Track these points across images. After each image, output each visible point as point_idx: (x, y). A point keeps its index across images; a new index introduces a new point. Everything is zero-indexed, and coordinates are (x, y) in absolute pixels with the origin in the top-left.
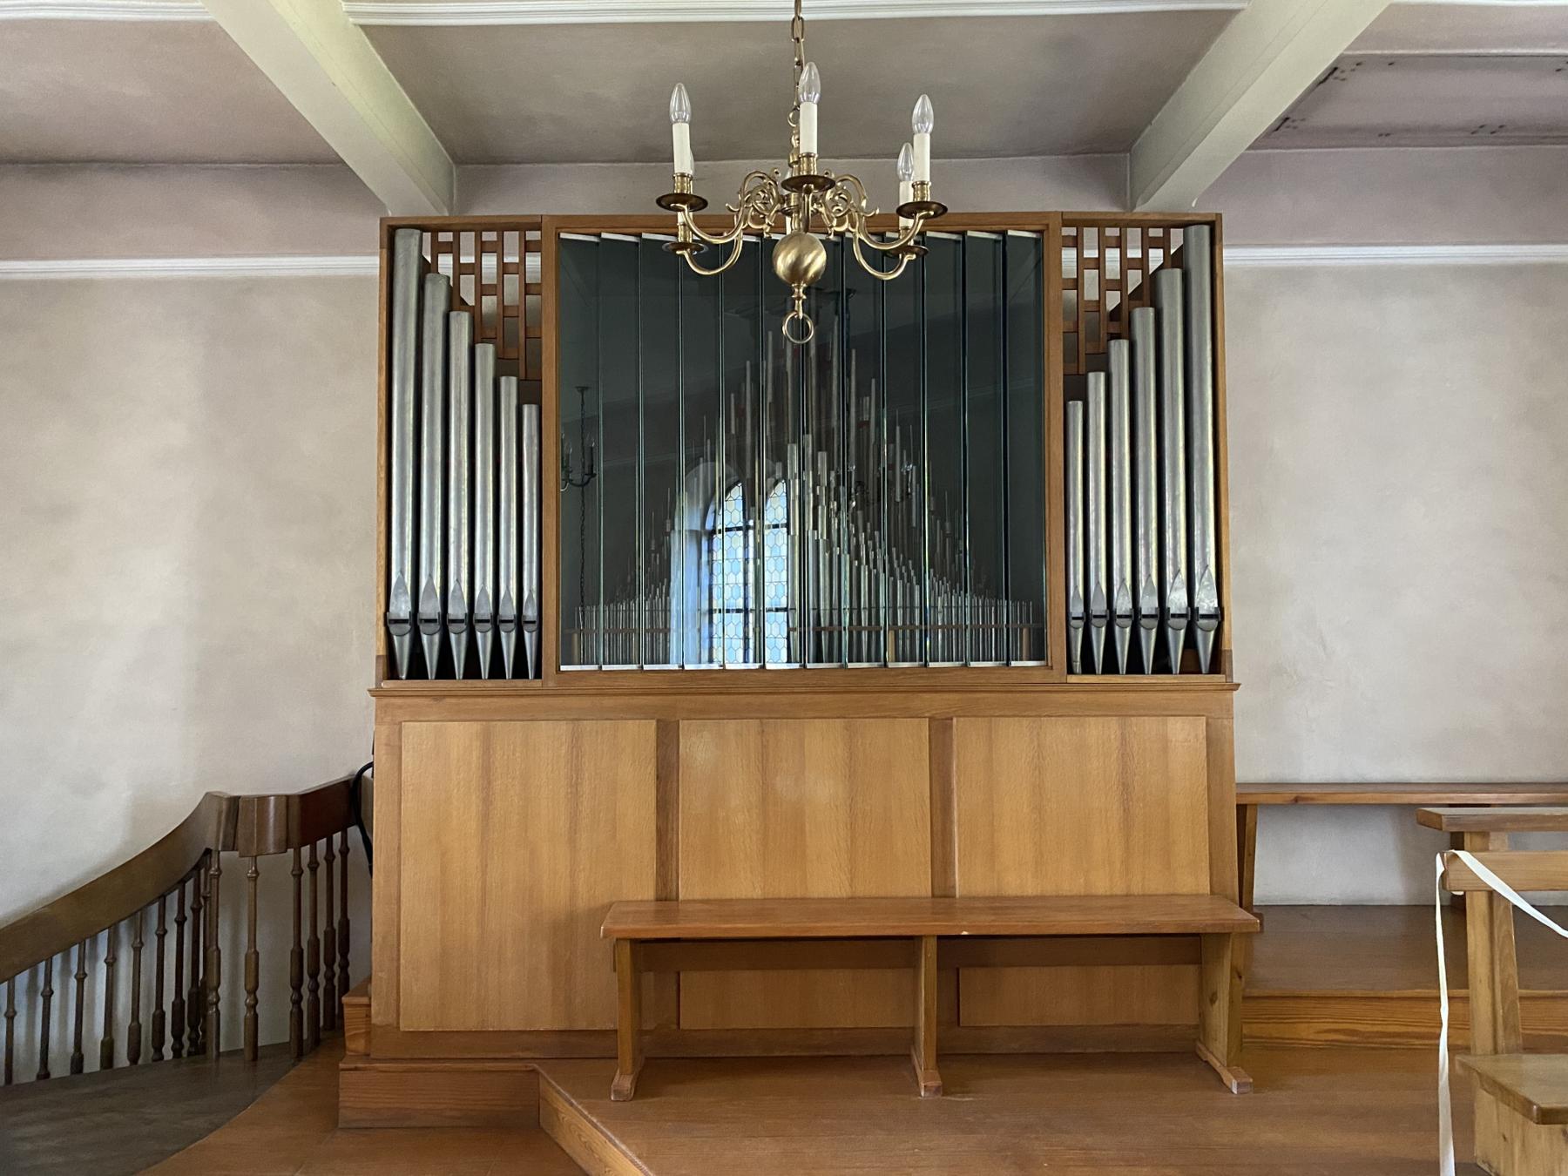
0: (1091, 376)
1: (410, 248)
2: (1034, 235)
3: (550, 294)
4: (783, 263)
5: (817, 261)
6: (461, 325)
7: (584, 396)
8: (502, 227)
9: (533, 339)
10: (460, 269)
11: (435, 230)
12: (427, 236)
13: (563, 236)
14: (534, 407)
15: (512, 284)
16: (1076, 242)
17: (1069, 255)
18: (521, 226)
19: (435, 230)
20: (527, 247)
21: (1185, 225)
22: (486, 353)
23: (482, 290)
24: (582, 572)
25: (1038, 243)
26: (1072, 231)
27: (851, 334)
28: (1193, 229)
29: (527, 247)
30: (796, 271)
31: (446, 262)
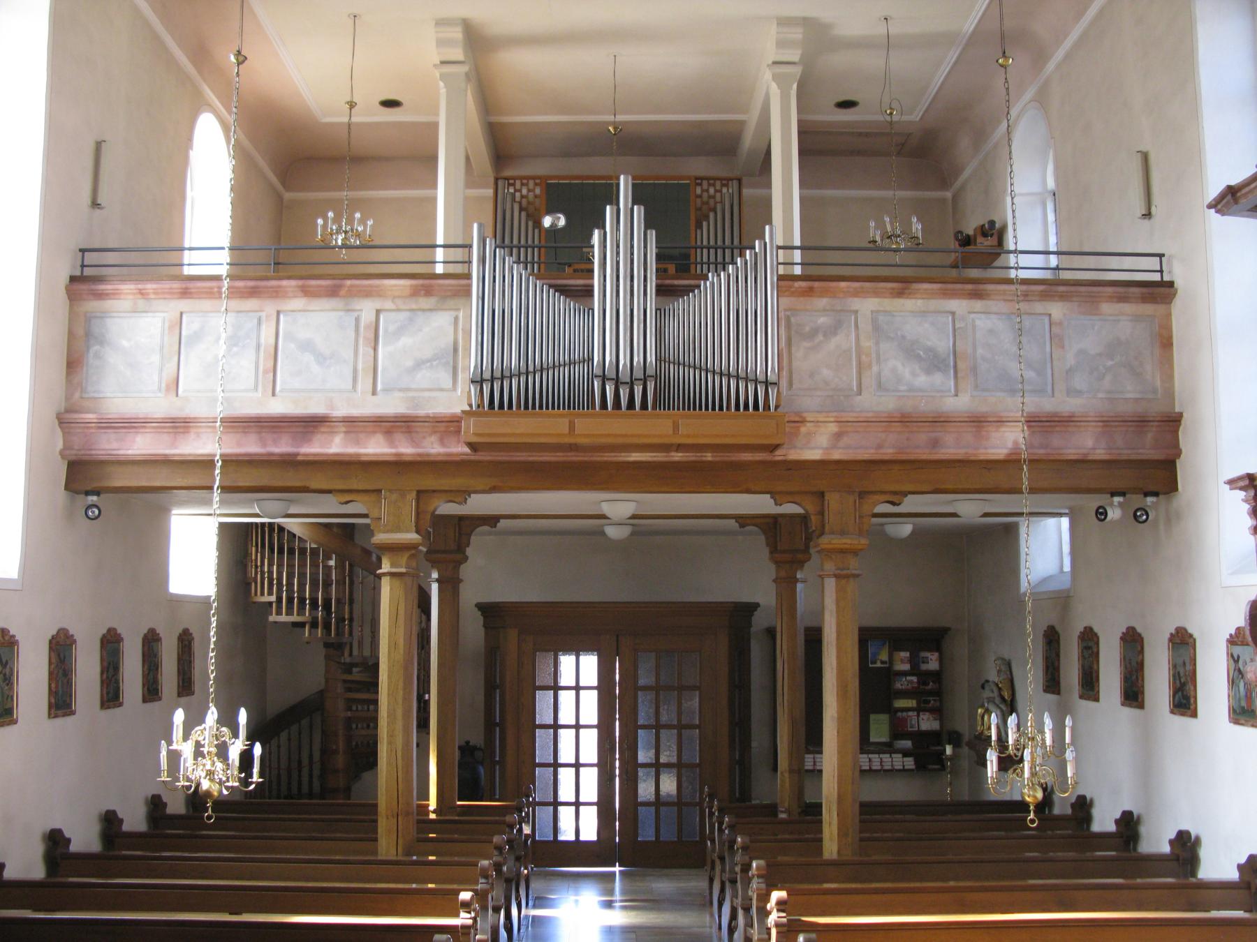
6: (516, 207)
22: (523, 214)
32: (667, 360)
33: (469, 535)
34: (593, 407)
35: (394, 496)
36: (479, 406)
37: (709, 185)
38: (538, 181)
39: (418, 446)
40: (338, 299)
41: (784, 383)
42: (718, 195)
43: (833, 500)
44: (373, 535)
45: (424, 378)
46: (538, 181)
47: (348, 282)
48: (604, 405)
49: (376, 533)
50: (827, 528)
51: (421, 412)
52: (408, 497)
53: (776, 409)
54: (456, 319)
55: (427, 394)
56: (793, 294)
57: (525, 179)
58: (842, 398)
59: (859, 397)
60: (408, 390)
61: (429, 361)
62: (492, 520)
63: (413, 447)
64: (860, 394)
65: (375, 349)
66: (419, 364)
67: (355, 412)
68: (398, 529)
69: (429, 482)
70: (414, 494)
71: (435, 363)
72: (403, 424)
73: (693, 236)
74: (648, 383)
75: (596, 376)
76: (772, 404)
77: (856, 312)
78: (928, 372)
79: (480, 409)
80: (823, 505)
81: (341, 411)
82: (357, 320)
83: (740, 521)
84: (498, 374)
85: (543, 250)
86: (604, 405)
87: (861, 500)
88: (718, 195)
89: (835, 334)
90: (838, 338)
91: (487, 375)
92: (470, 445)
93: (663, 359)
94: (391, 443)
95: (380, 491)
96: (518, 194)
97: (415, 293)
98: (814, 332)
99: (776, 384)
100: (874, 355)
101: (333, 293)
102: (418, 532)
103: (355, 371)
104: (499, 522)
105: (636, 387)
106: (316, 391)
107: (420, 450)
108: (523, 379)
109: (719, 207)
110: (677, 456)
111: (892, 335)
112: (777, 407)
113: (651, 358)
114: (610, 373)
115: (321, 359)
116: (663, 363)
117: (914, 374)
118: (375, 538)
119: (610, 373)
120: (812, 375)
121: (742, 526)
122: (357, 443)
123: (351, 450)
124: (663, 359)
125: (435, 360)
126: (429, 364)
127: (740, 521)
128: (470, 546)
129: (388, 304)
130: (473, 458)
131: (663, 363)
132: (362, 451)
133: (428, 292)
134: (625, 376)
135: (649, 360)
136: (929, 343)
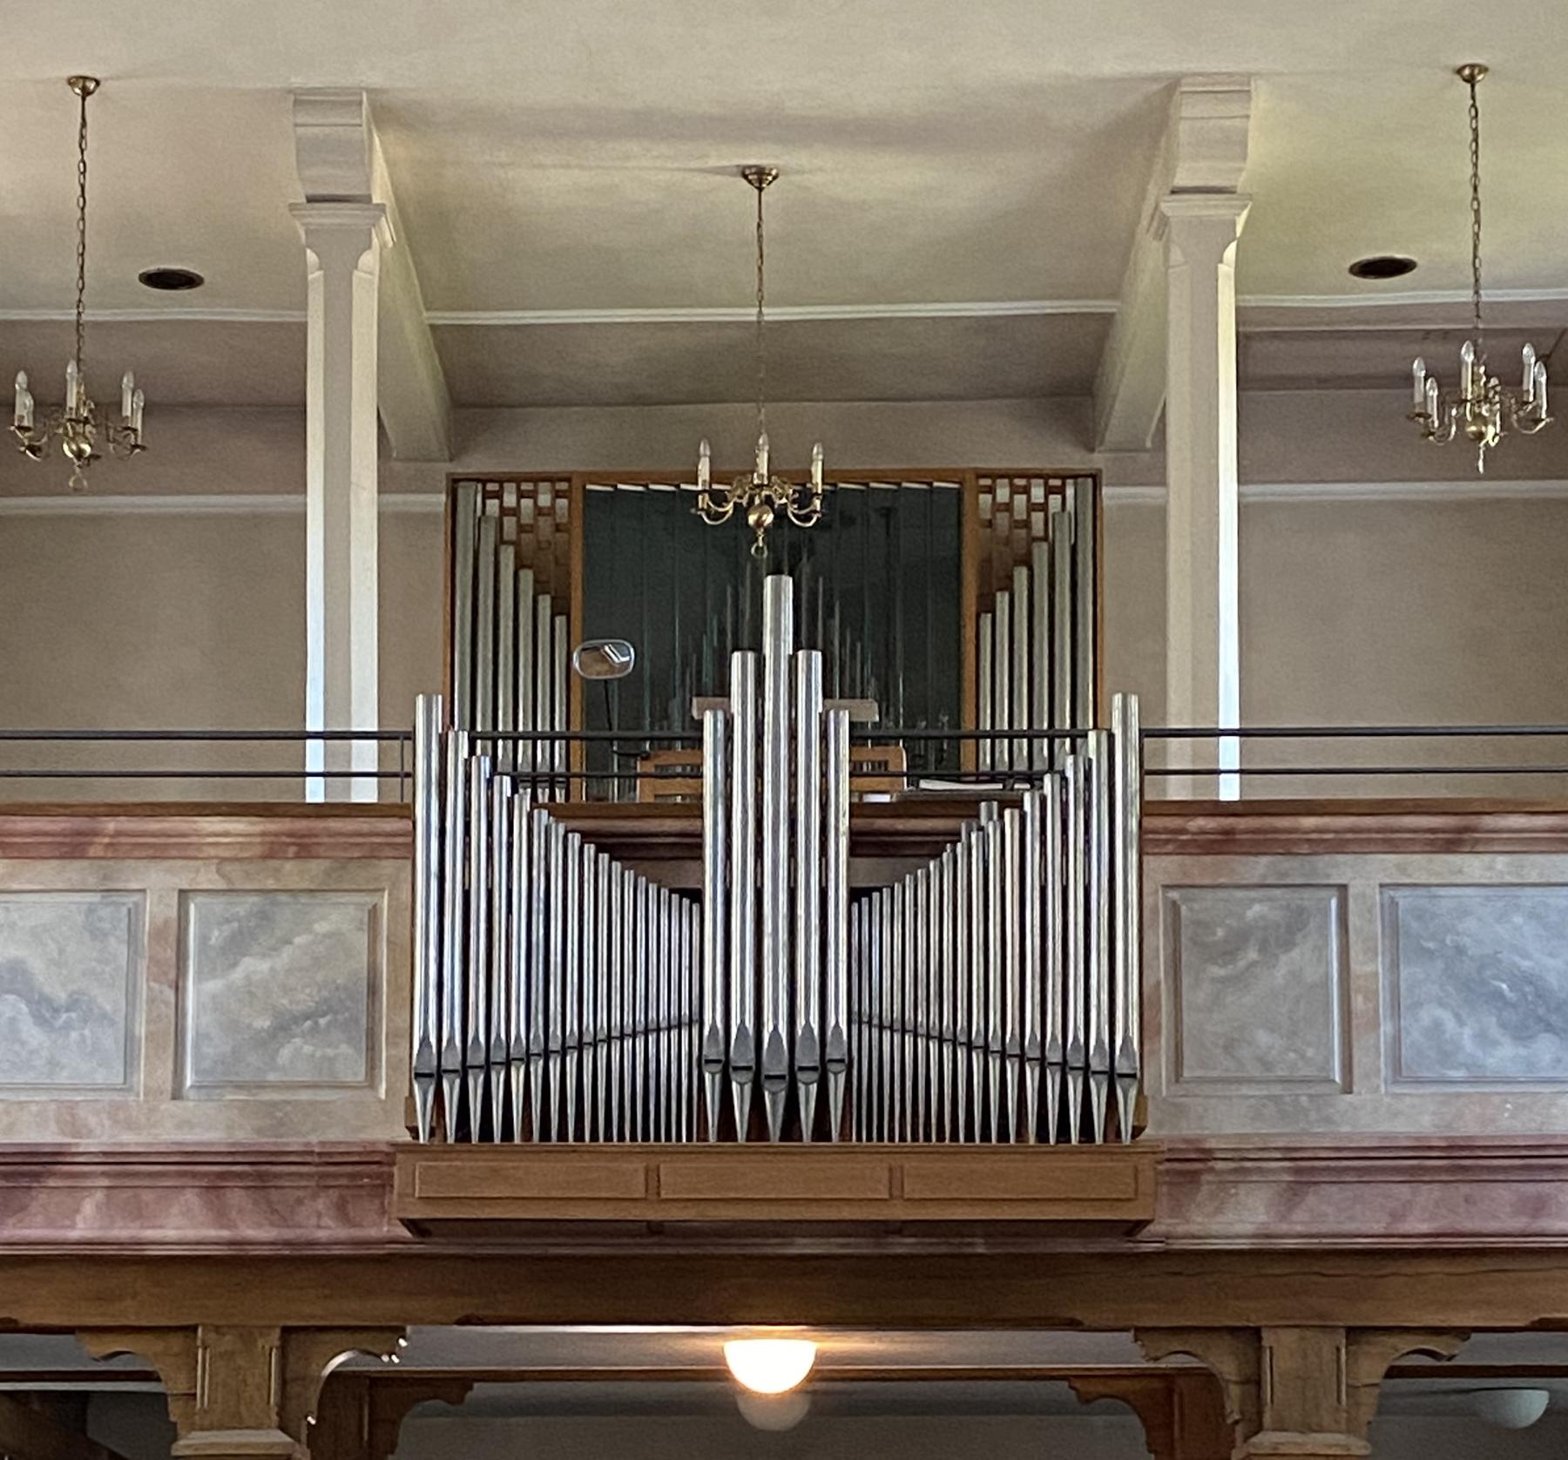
0: (999, 594)
1: (470, 497)
2: (956, 486)
3: (577, 532)
4: (752, 519)
5: (769, 518)
6: (508, 555)
7: (86, 103)
8: (537, 479)
9: (563, 564)
10: (504, 511)
11: (484, 482)
12: (480, 486)
13: (589, 487)
14: (564, 618)
15: (545, 524)
16: (991, 490)
17: (985, 499)
18: (551, 479)
19: (484, 482)
20: (557, 495)
21: (1075, 477)
22: (527, 576)
23: (521, 528)
24: (1477, 235)
25: (959, 494)
26: (988, 482)
27: (228, 1192)
28: (1080, 480)
29: (557, 495)
30: (759, 523)
31: (493, 505)
32: (875, 1021)
33: (395, 1424)
34: (703, 1136)
35: (228, 1342)
36: (432, 1133)
37: (1014, 491)
38: (563, 486)
39: (285, 1222)
40: (85, 863)
41: (1159, 1071)
42: (1038, 517)
43: (1283, 1348)
44: (175, 1438)
45: (295, 1055)
46: (563, 486)
47: (111, 825)
48: (727, 1128)
49: (181, 1432)
50: (1267, 1419)
51: (294, 1142)
52: (260, 1343)
53: (1134, 1136)
54: (374, 913)
55: (304, 1096)
56: (1183, 849)
57: (527, 482)
58: (1304, 1099)
59: (1348, 1097)
60: (262, 1086)
61: (307, 1017)
62: (452, 1386)
63: (272, 1224)
64: (1348, 1089)
65: (179, 988)
66: (284, 1026)
67: (130, 1140)
68: (236, 1422)
69: (310, 1310)
70: (275, 1337)
71: (322, 1021)
72: (247, 1168)
73: (969, 633)
74: (832, 1077)
75: (708, 1062)
76: (1127, 1123)
77: (1343, 888)
78: (1521, 1034)
79: (436, 1141)
80: (1259, 1362)
81: (100, 1136)
82: (134, 915)
83: (1078, 1384)
84: (477, 1058)
85: (575, 744)
86: (727, 1128)
87: (1352, 1348)
88: (1038, 517)
89: (1288, 945)
90: (1295, 954)
91: (452, 1061)
92: (410, 1224)
93: (865, 1019)
94: (221, 1216)
95: (194, 1329)
96: (509, 523)
97: (273, 851)
98: (1240, 938)
99: (1133, 1076)
100: (1383, 997)
101: (73, 848)
102: (283, 1428)
103: (129, 1038)
104: (471, 1388)
105: (802, 1088)
106: (35, 1088)
107: (289, 1234)
108: (537, 1067)
109: (1040, 553)
110: (903, 1246)
111: (1431, 945)
112: (1137, 1131)
113: (839, 1017)
114: (742, 1056)
115: (45, 1010)
116: (865, 1029)
117: (1482, 1038)
118: (182, 1442)
119: (742, 1056)
120: (1229, 1047)
121: (1085, 1399)
122: (138, 1214)
123: (123, 1231)
124: (865, 1019)
125: (323, 1016)
126: (308, 1023)
127: (1078, 1384)
128: (397, 1450)
129: (208, 878)
130: (418, 1249)
131: (865, 1029)
132: (150, 1234)
133: (305, 849)
134: (775, 1065)
135: (832, 1022)
136: (1526, 964)
